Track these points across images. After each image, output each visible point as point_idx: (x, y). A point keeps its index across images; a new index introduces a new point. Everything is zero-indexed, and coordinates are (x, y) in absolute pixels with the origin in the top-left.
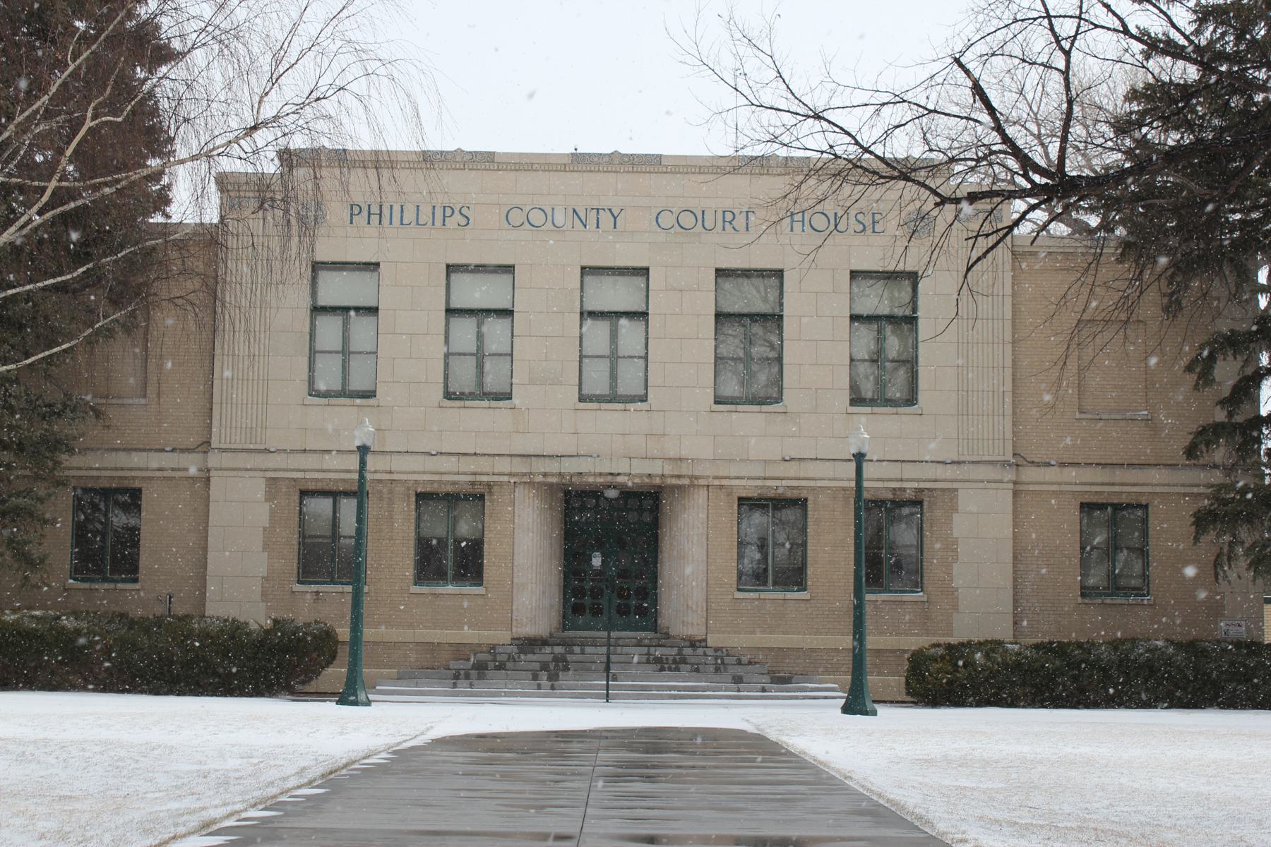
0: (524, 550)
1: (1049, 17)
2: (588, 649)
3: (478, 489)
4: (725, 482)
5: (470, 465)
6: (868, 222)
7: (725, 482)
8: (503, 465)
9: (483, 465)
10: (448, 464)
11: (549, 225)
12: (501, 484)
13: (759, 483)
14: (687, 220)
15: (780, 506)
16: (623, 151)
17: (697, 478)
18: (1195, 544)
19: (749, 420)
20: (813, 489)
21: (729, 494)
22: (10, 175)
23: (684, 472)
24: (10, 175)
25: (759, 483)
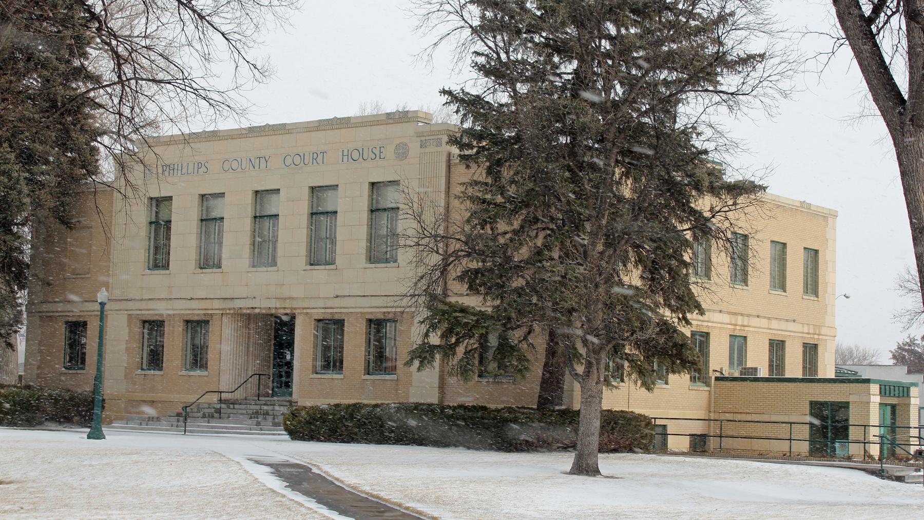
0: (228, 351)
1: (790, 439)
2: (236, 406)
3: (206, 318)
4: (308, 311)
5: (203, 305)
6: (377, 153)
7: (308, 311)
8: (217, 304)
9: (207, 305)
10: (195, 305)
11: (239, 169)
12: (216, 314)
13: (323, 311)
14: (297, 160)
15: (331, 326)
16: (271, 123)
17: (295, 309)
18: (71, 228)
19: (321, 273)
20: (347, 313)
21: (310, 318)
22: (585, 342)
23: (287, 306)
24: (585, 342)
25: (323, 311)
